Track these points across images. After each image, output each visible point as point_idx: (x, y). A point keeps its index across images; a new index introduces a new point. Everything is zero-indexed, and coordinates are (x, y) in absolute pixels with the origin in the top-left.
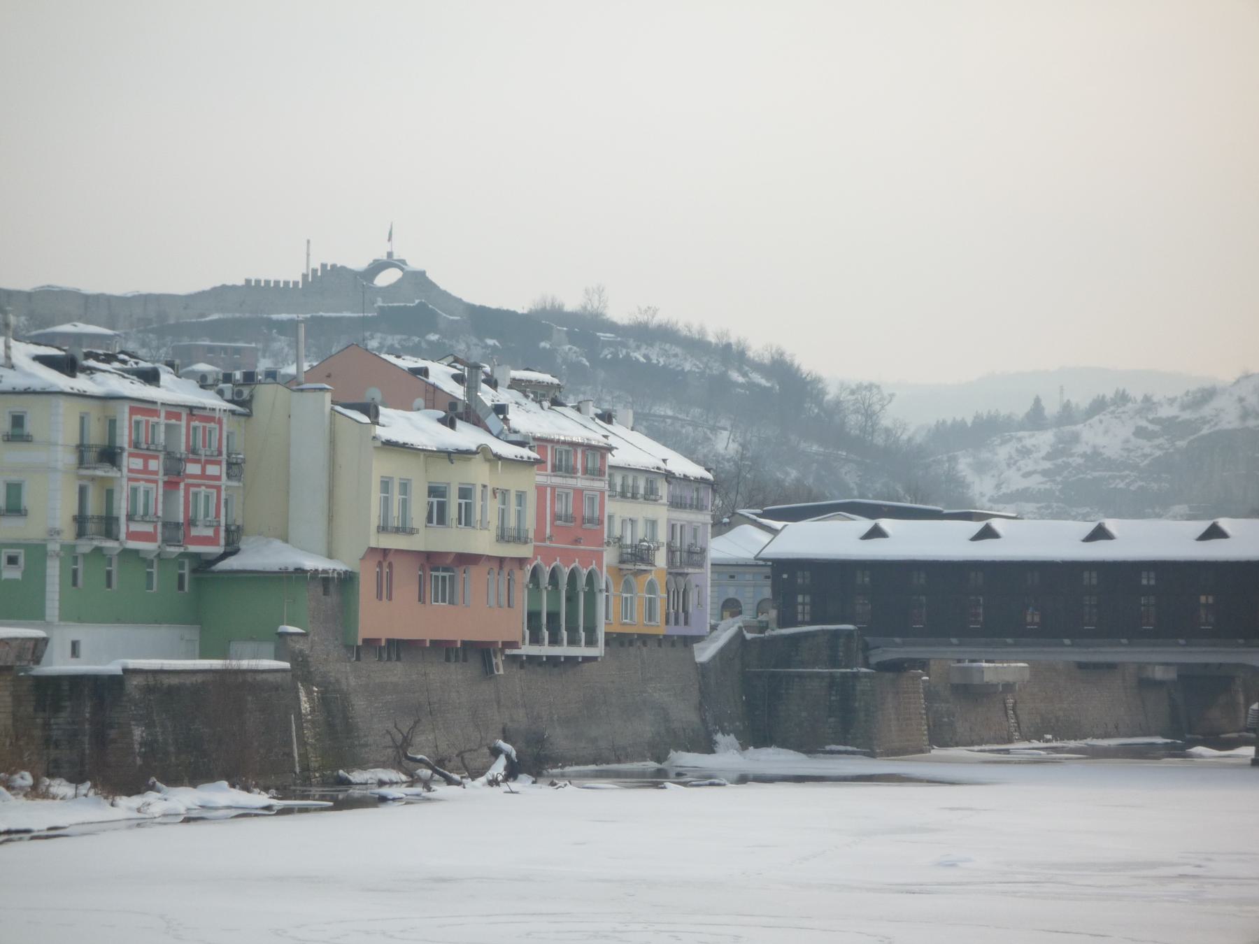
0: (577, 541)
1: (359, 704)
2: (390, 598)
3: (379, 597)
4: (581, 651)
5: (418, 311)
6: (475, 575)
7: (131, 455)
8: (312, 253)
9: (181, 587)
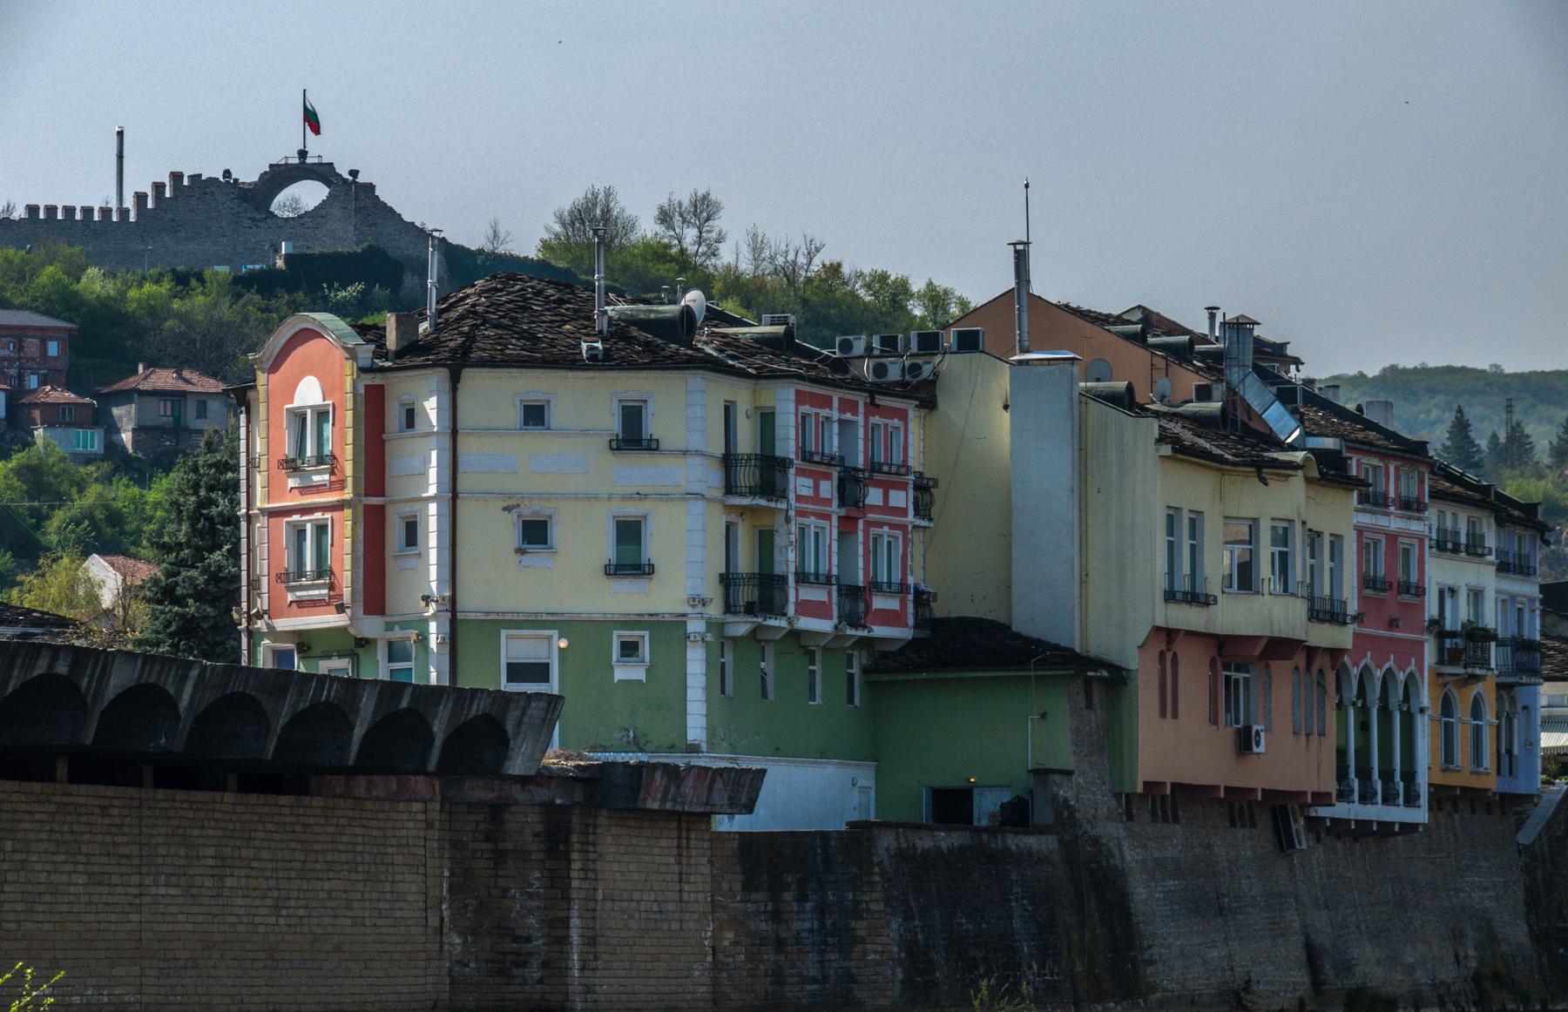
0: (1392, 624)
1: (1140, 891)
2: (1175, 715)
3: (1163, 715)
4: (1398, 814)
5: (346, 258)
6: (1283, 673)
7: (801, 472)
8: (114, 159)
9: (851, 700)
